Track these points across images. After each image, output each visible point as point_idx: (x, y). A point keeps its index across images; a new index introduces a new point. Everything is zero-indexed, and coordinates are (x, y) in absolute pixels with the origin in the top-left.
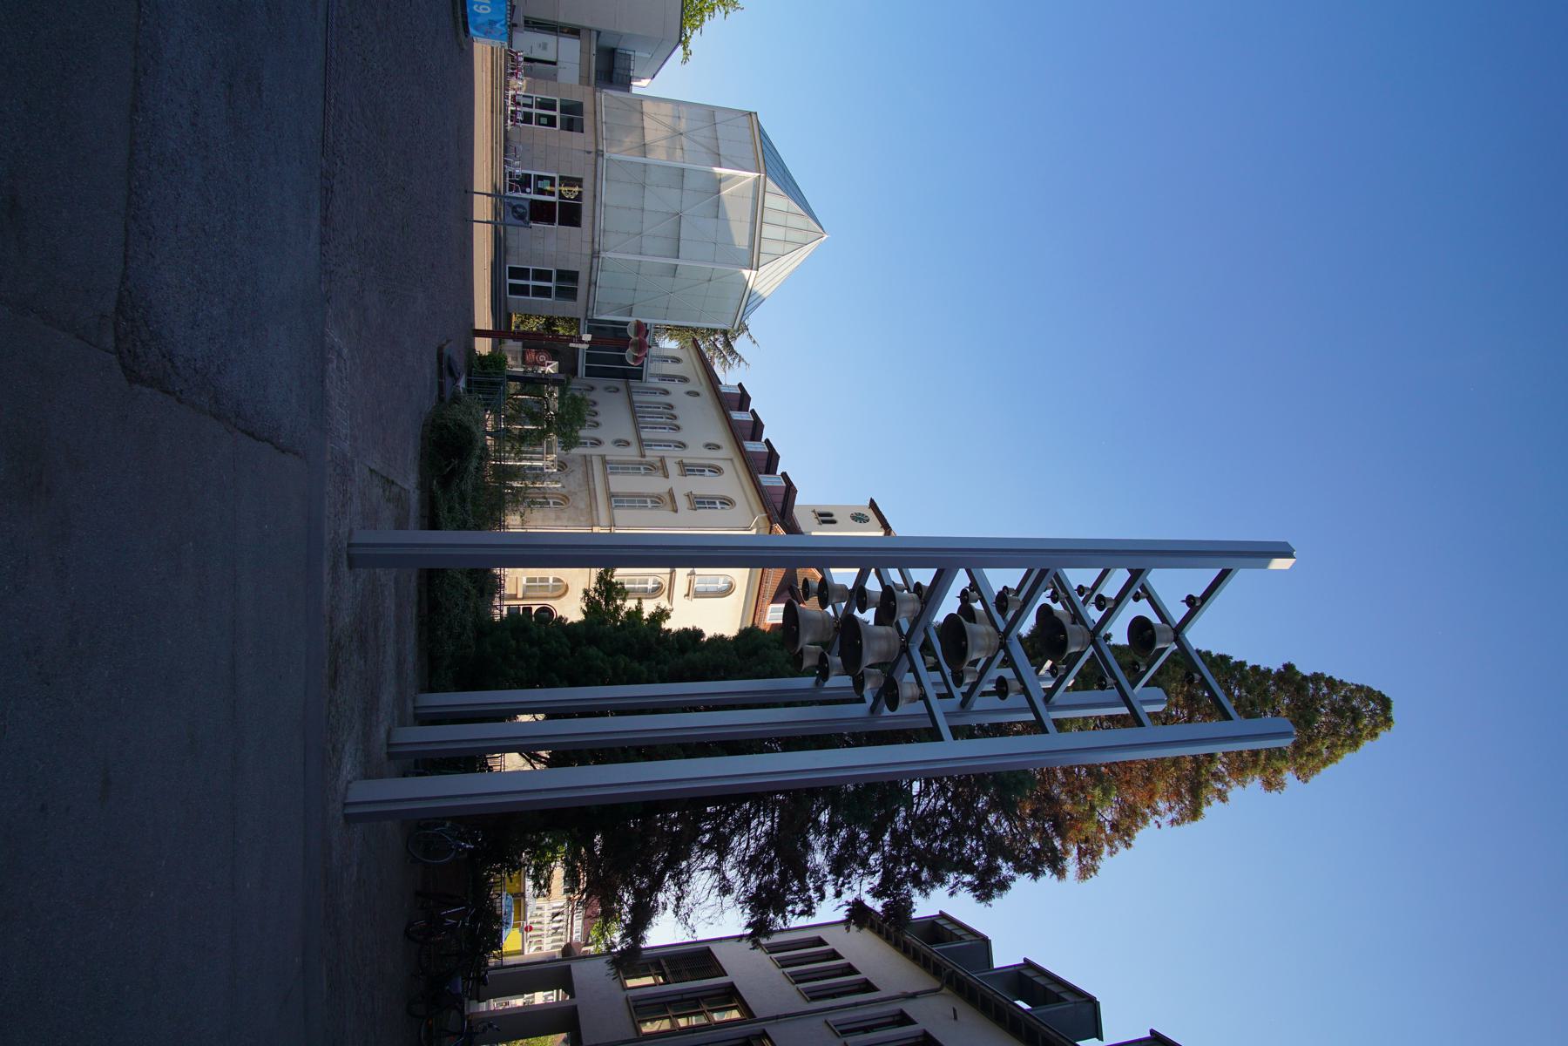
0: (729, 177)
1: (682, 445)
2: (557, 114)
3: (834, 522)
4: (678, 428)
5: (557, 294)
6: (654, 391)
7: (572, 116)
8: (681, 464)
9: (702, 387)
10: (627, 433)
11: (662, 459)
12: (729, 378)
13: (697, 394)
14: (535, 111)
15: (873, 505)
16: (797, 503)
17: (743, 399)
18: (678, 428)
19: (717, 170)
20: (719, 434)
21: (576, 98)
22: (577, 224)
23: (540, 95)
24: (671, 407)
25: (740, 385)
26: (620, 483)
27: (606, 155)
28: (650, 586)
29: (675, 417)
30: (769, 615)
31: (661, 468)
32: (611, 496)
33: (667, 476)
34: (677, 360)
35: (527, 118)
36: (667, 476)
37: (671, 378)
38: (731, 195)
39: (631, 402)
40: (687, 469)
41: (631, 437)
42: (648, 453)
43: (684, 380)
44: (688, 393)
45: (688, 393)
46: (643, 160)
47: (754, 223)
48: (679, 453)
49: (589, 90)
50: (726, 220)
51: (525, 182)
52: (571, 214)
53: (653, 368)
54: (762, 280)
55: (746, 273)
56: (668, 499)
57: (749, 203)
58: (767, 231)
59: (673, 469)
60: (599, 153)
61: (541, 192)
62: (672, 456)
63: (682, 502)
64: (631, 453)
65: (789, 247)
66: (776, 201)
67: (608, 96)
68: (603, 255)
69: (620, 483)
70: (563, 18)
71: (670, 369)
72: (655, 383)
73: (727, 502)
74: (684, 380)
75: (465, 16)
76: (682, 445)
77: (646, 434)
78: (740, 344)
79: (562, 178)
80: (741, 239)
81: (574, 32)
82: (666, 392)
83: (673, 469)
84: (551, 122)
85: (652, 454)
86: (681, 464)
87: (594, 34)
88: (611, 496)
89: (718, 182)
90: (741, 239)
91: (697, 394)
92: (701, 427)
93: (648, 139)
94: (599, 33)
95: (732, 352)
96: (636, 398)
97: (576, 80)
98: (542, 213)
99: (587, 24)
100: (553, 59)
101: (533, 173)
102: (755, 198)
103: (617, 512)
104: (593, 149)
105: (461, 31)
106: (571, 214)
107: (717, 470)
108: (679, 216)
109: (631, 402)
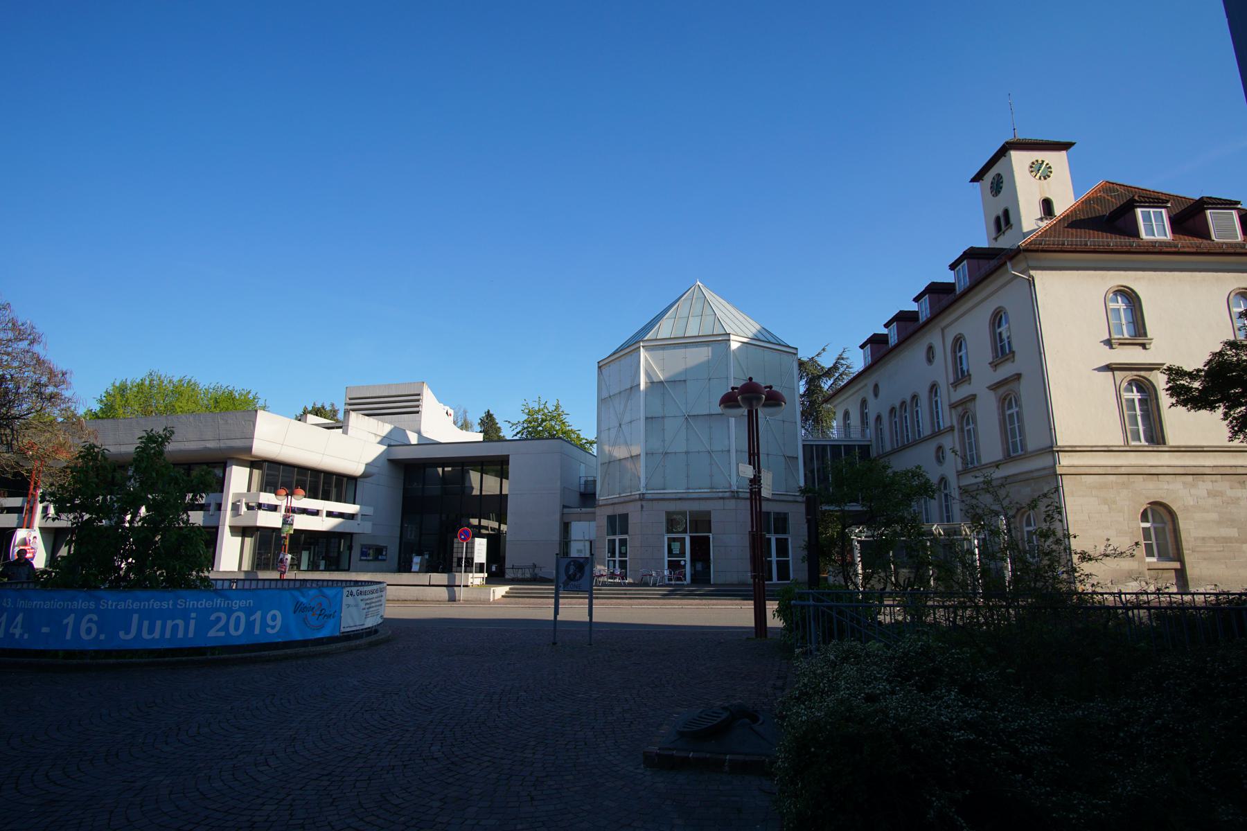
0: (648, 374)
1: (934, 388)
2: (617, 538)
3: (1006, 212)
4: (915, 397)
5: (785, 532)
6: (879, 431)
7: (618, 523)
8: (956, 384)
9: (869, 382)
10: (929, 449)
11: (953, 406)
12: (857, 361)
13: (876, 386)
14: (617, 558)
15: (978, 178)
16: (986, 245)
17: (876, 341)
18: (915, 397)
19: (642, 387)
20: (916, 352)
21: (604, 522)
22: (709, 513)
23: (607, 555)
24: (893, 410)
25: (862, 347)
26: (990, 446)
27: (643, 491)
28: (1136, 396)
29: (903, 403)
30: (1158, 237)
31: (964, 407)
32: (1009, 458)
33: (973, 398)
34: (846, 415)
35: (623, 565)
36: (973, 398)
37: (864, 417)
38: (663, 370)
39: (894, 452)
40: (962, 377)
41: (931, 447)
42: (948, 424)
43: (864, 403)
44: (876, 395)
45: (876, 395)
46: (643, 458)
47: (686, 345)
48: (943, 389)
49: (598, 510)
50: (686, 371)
51: (674, 566)
52: (701, 522)
53: (856, 435)
54: (741, 332)
55: (734, 345)
56: (1001, 391)
57: (667, 353)
58: (692, 331)
59: (964, 391)
60: (642, 498)
61: (683, 554)
62: (947, 396)
63: (1006, 371)
64: (949, 442)
65: (708, 311)
66: (665, 329)
67: (601, 497)
68: (735, 488)
69: (990, 446)
70: (556, 536)
71: (855, 420)
72: (870, 432)
73: (998, 318)
74: (864, 403)
75: (286, 645)
76: (934, 388)
77: (926, 430)
78: (826, 362)
79: (669, 531)
80: (702, 355)
81: (566, 527)
82: (879, 418)
83: (964, 391)
84: (623, 543)
85: (948, 418)
86: (956, 384)
87: (566, 510)
88: (1009, 458)
89: (653, 384)
90: (703, 354)
91: (876, 386)
92: (913, 371)
93: (627, 455)
94: (564, 507)
95: (835, 367)
96: (888, 448)
97: (592, 523)
98: (701, 549)
99: (558, 516)
100: (588, 544)
101: (667, 559)
102: (663, 347)
103: (1031, 445)
104: (639, 503)
105: (373, 638)
106: (701, 522)
107: (958, 342)
108: (689, 418)
109: (894, 452)
